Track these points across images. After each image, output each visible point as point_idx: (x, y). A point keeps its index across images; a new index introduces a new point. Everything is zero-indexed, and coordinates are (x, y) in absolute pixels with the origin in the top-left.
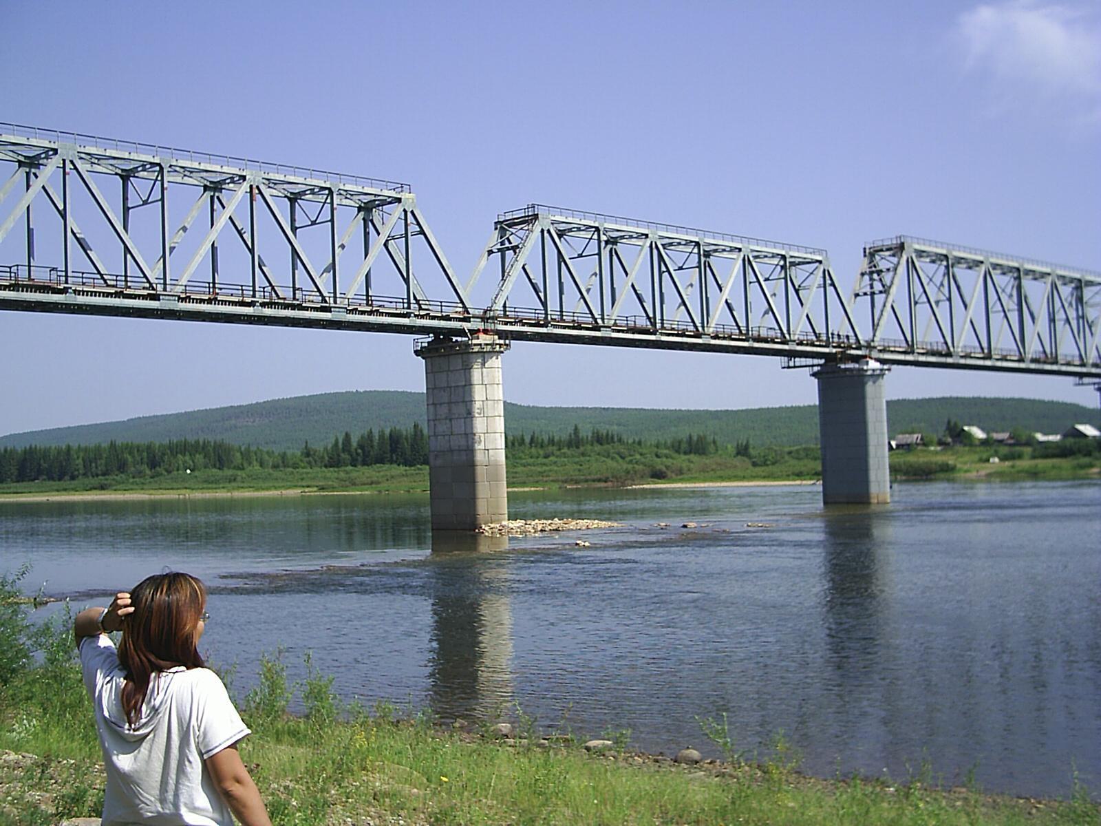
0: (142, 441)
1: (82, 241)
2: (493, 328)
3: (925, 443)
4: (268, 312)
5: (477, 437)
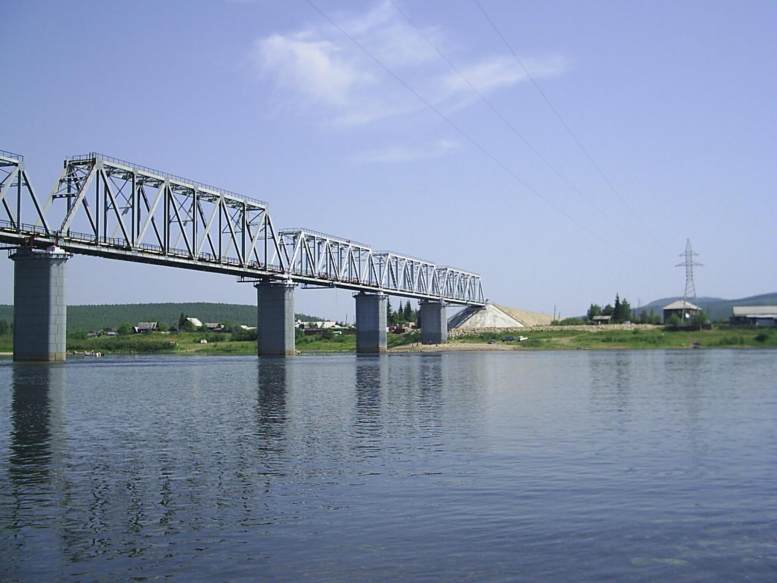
3: (159, 329)
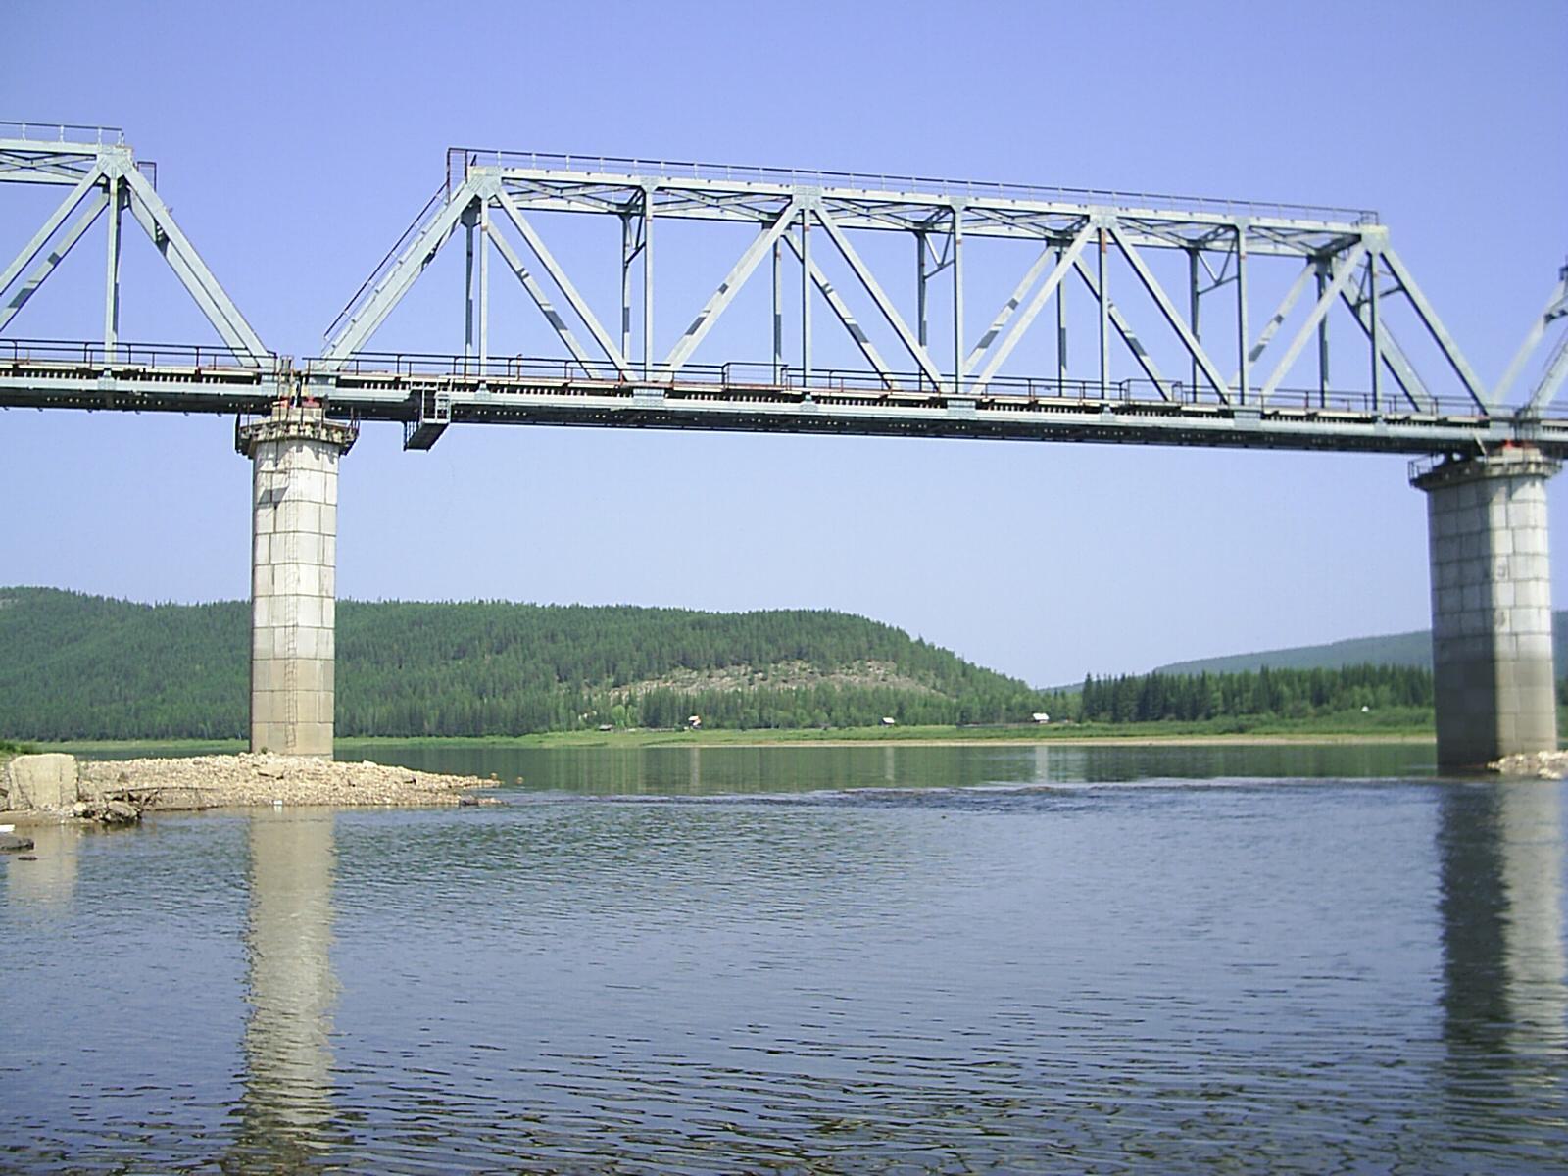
0: (1308, 667)
1: (852, 329)
2: (1530, 437)
4: (1125, 420)
5: (1497, 614)
